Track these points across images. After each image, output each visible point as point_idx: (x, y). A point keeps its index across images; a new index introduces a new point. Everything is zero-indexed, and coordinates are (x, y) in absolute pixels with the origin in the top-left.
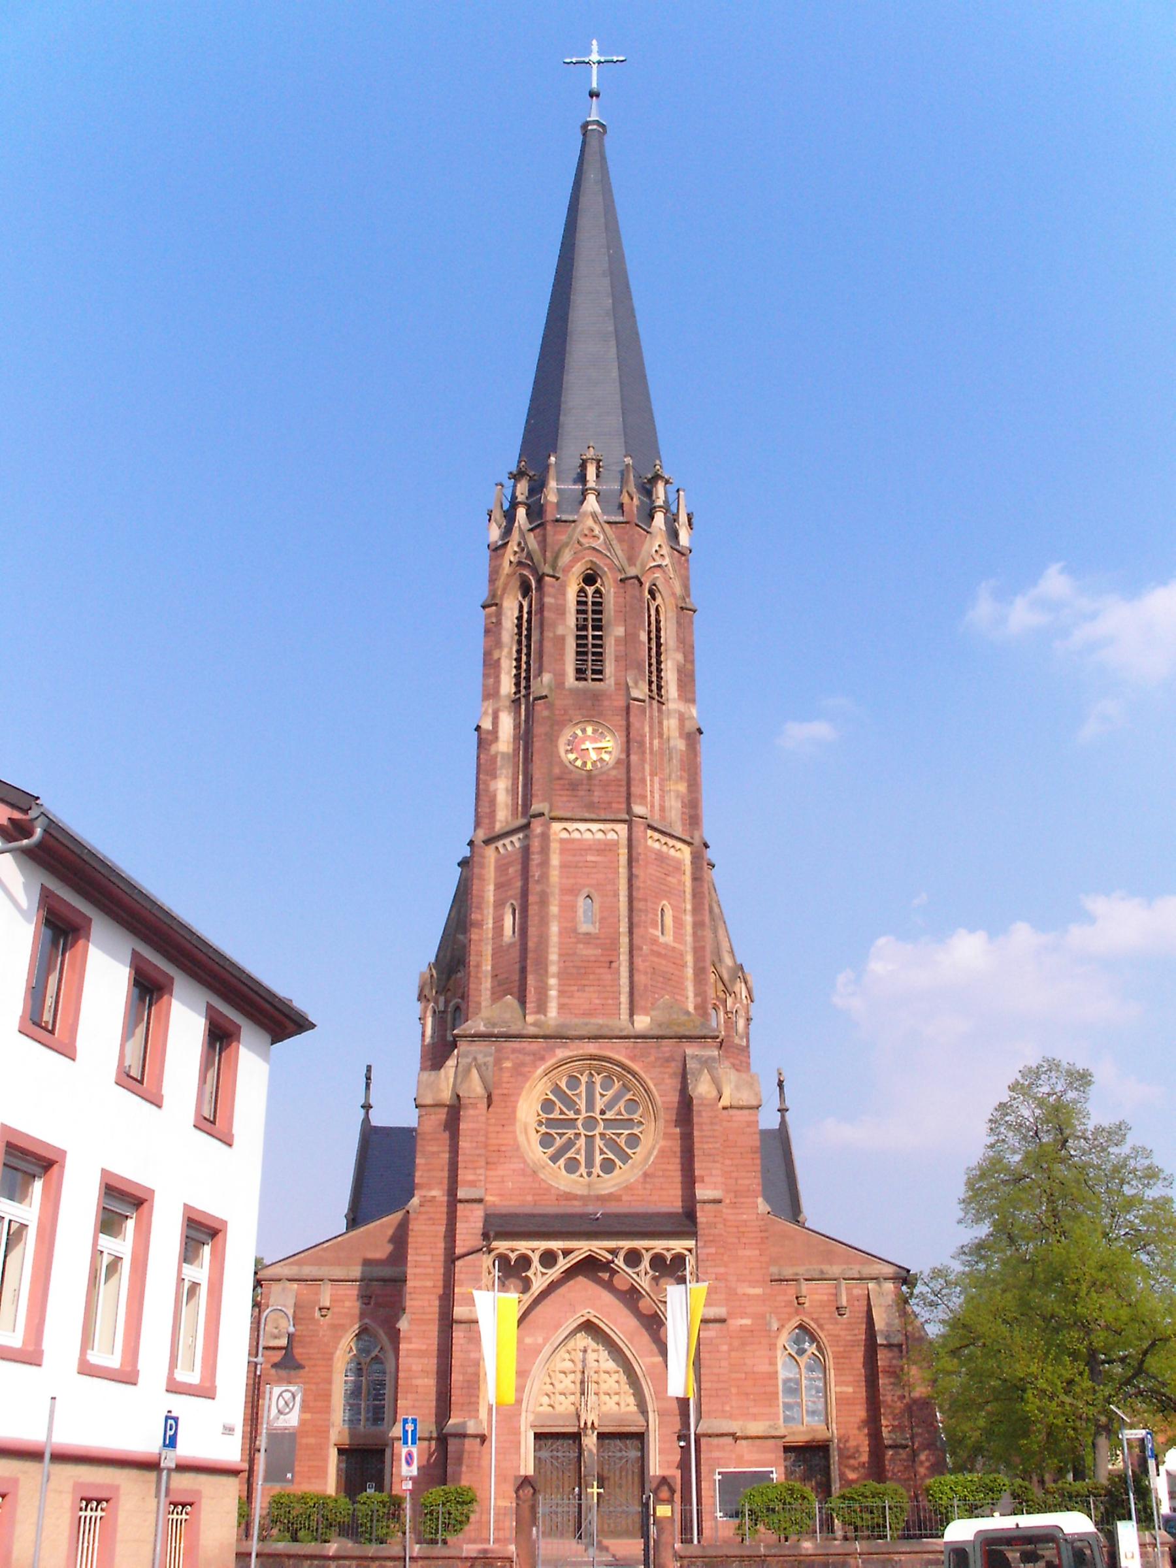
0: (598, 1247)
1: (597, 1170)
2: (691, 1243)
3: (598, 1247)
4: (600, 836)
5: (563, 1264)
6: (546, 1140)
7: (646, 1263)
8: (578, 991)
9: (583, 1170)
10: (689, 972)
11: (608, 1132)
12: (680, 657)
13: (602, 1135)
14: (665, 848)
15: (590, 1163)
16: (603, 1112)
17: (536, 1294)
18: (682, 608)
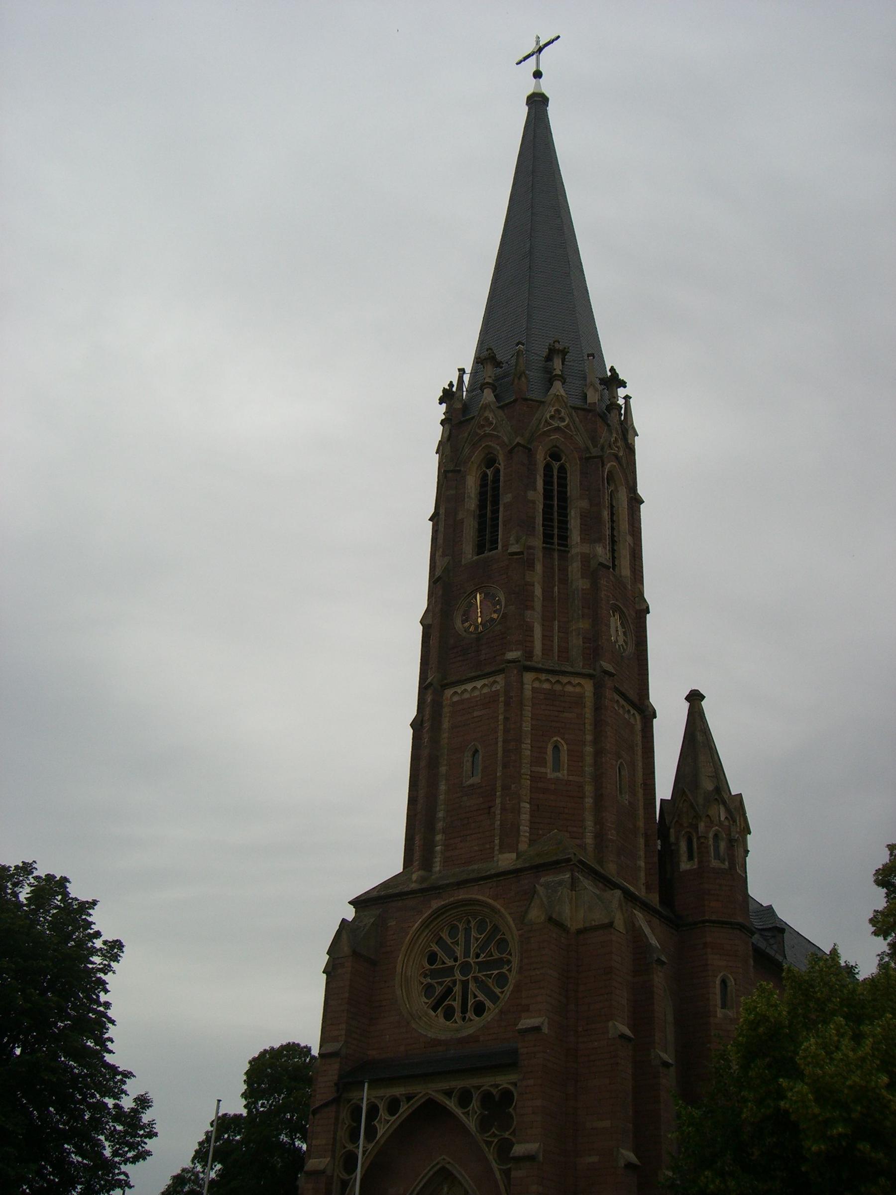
0: (432, 1090)
1: (470, 1014)
2: (513, 1077)
3: (432, 1090)
4: (485, 691)
5: (404, 1109)
6: (428, 990)
7: (475, 1104)
8: (461, 842)
9: (457, 1015)
10: (589, 801)
11: (479, 975)
12: (584, 504)
13: (475, 979)
14: (558, 687)
15: (464, 1010)
16: (478, 956)
17: (382, 1142)
18: (588, 459)
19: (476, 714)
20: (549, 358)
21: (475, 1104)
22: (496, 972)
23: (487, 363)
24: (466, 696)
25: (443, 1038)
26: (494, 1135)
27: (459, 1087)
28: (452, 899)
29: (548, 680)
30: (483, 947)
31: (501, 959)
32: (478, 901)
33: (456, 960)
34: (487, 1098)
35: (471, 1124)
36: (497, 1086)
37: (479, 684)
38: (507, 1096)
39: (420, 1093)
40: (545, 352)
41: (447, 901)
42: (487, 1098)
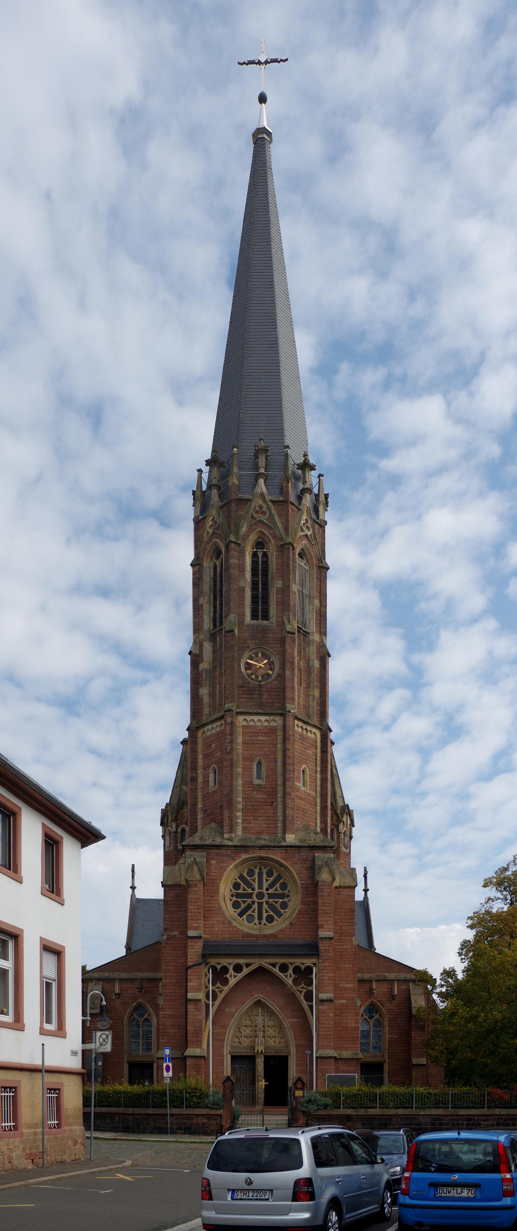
0: (265, 962)
2: (314, 961)
3: (265, 962)
5: (245, 971)
7: (291, 971)
11: (271, 900)
13: (267, 903)
15: (260, 918)
19: (260, 738)
20: (256, 456)
21: (291, 971)
22: (281, 900)
23: (262, 453)
24: (252, 724)
25: (254, 933)
26: (303, 988)
27: (281, 962)
28: (255, 855)
29: (274, 720)
30: (271, 886)
31: (283, 894)
32: (272, 859)
33: (253, 889)
34: (297, 970)
35: (290, 981)
36: (303, 964)
37: (263, 718)
38: (309, 970)
39: (255, 963)
40: (252, 453)
41: (252, 855)
42: (297, 970)
